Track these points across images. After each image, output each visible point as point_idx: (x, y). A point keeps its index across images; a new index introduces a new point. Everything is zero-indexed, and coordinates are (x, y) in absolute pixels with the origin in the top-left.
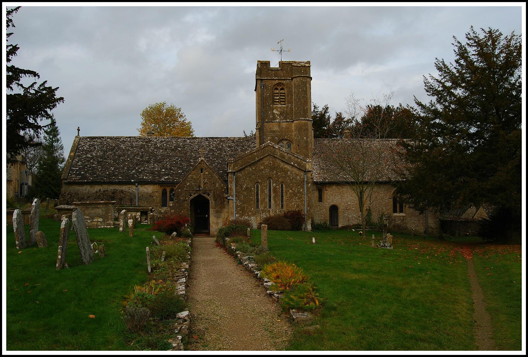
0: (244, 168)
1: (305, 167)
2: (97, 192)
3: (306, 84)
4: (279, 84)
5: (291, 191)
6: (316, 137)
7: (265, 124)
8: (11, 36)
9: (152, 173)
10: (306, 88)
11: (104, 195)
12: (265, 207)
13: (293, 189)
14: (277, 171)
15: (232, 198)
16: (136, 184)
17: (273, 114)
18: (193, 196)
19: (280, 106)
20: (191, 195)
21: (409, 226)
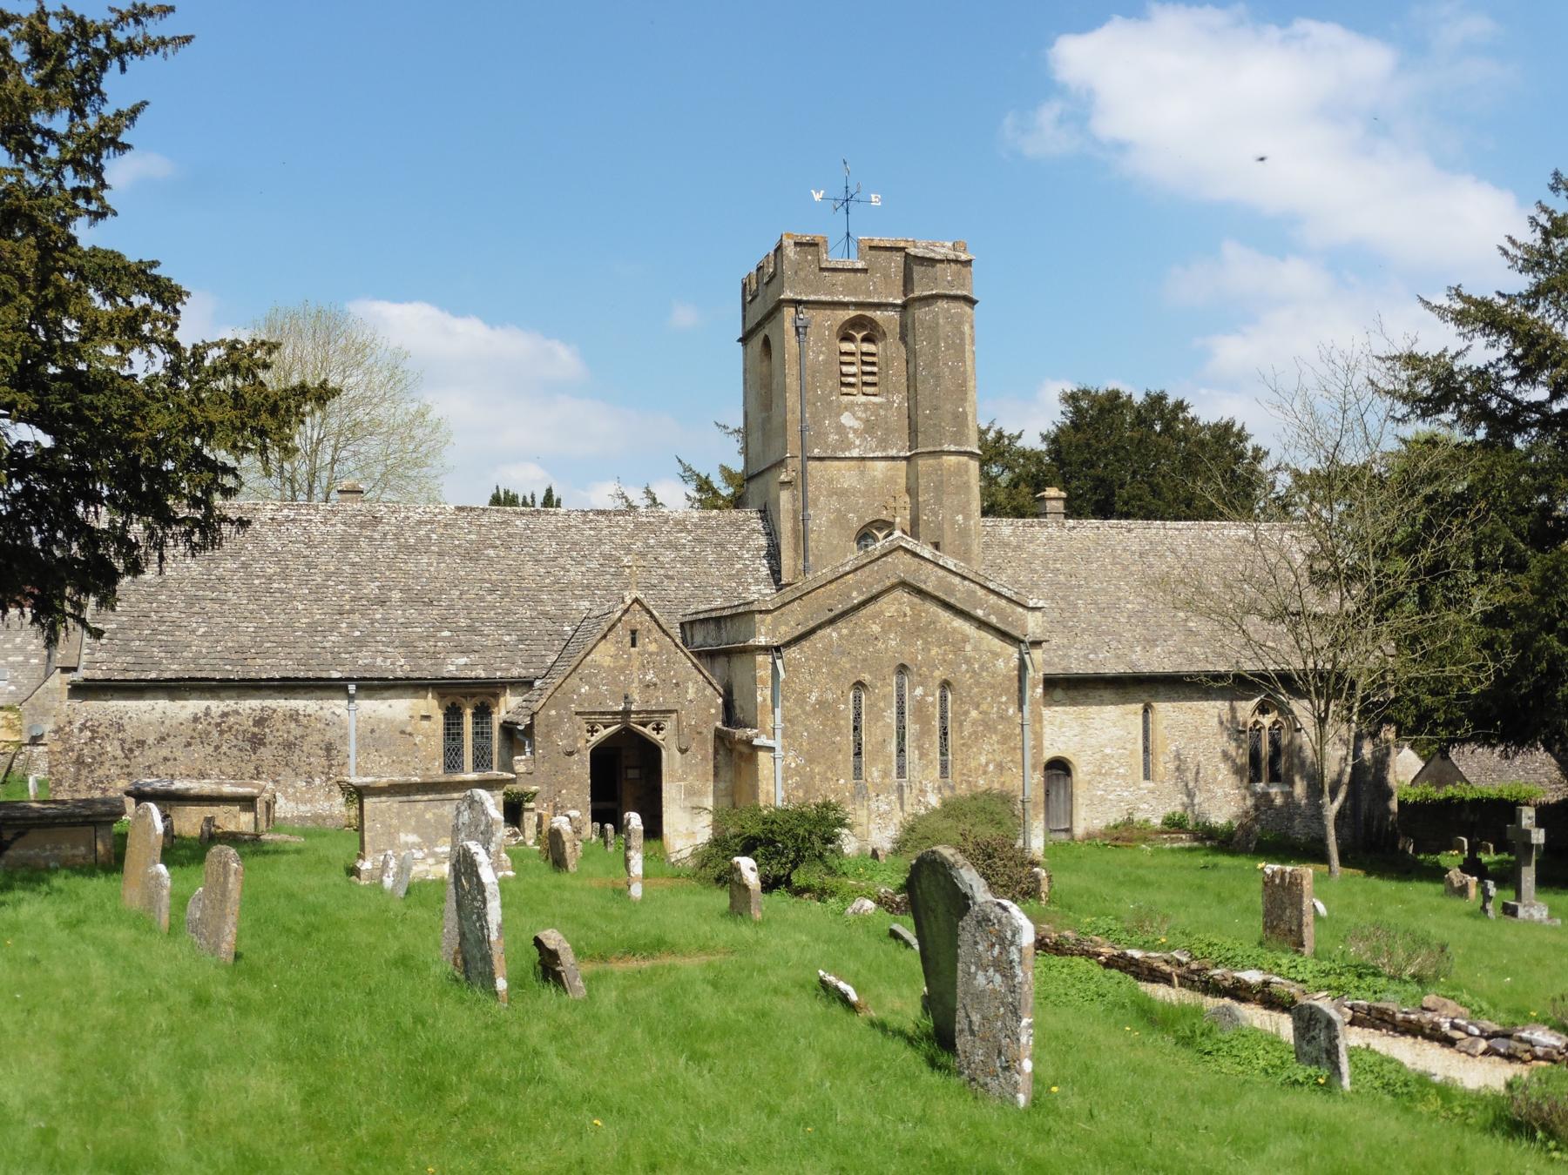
0: (813, 631)
1: (1024, 626)
2: (196, 719)
3: (961, 323)
4: (857, 323)
5: (974, 714)
6: (985, 513)
7: (812, 465)
8: (140, 116)
10: (962, 339)
11: (221, 733)
12: (886, 774)
13: (984, 707)
14: (926, 642)
15: (770, 743)
16: (352, 688)
17: (841, 429)
18: (603, 733)
19: (863, 399)
20: (592, 731)
21: (1213, 820)
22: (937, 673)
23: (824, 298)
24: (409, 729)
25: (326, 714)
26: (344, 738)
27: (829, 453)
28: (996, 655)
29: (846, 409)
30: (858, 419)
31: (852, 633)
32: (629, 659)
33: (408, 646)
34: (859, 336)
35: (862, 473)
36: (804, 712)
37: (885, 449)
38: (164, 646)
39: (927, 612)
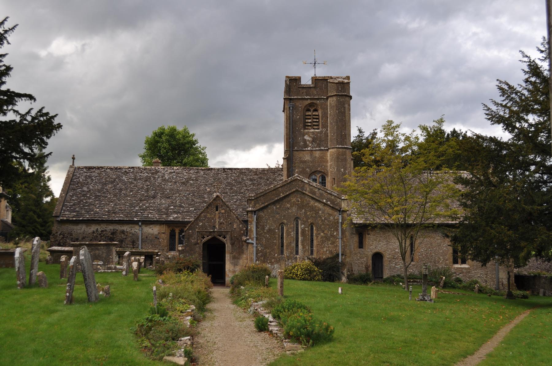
1: (340, 205)
2: (94, 232)
3: (344, 104)
4: (311, 105)
5: (322, 234)
7: (295, 152)
9: (159, 211)
10: (344, 109)
11: (101, 236)
14: (305, 210)
16: (140, 223)
17: (305, 141)
19: (312, 130)
20: (203, 238)
22: (309, 220)
23: (299, 97)
24: (158, 237)
25: (133, 231)
26: (138, 239)
27: (300, 149)
28: (330, 215)
29: (306, 134)
30: (310, 137)
31: (280, 207)
32: (215, 215)
33: (159, 211)
34: (312, 110)
35: (311, 155)
36: (264, 232)
37: (320, 147)
38: (85, 210)
39: (306, 200)
